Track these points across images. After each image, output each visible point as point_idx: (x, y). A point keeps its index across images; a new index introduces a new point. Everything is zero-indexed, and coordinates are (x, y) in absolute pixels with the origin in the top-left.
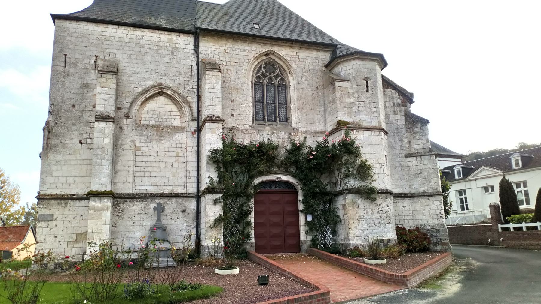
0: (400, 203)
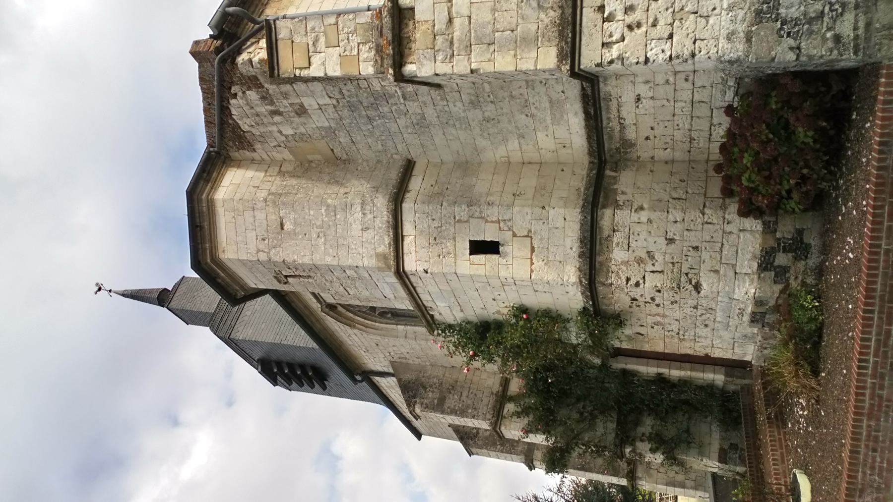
0: (624, 114)
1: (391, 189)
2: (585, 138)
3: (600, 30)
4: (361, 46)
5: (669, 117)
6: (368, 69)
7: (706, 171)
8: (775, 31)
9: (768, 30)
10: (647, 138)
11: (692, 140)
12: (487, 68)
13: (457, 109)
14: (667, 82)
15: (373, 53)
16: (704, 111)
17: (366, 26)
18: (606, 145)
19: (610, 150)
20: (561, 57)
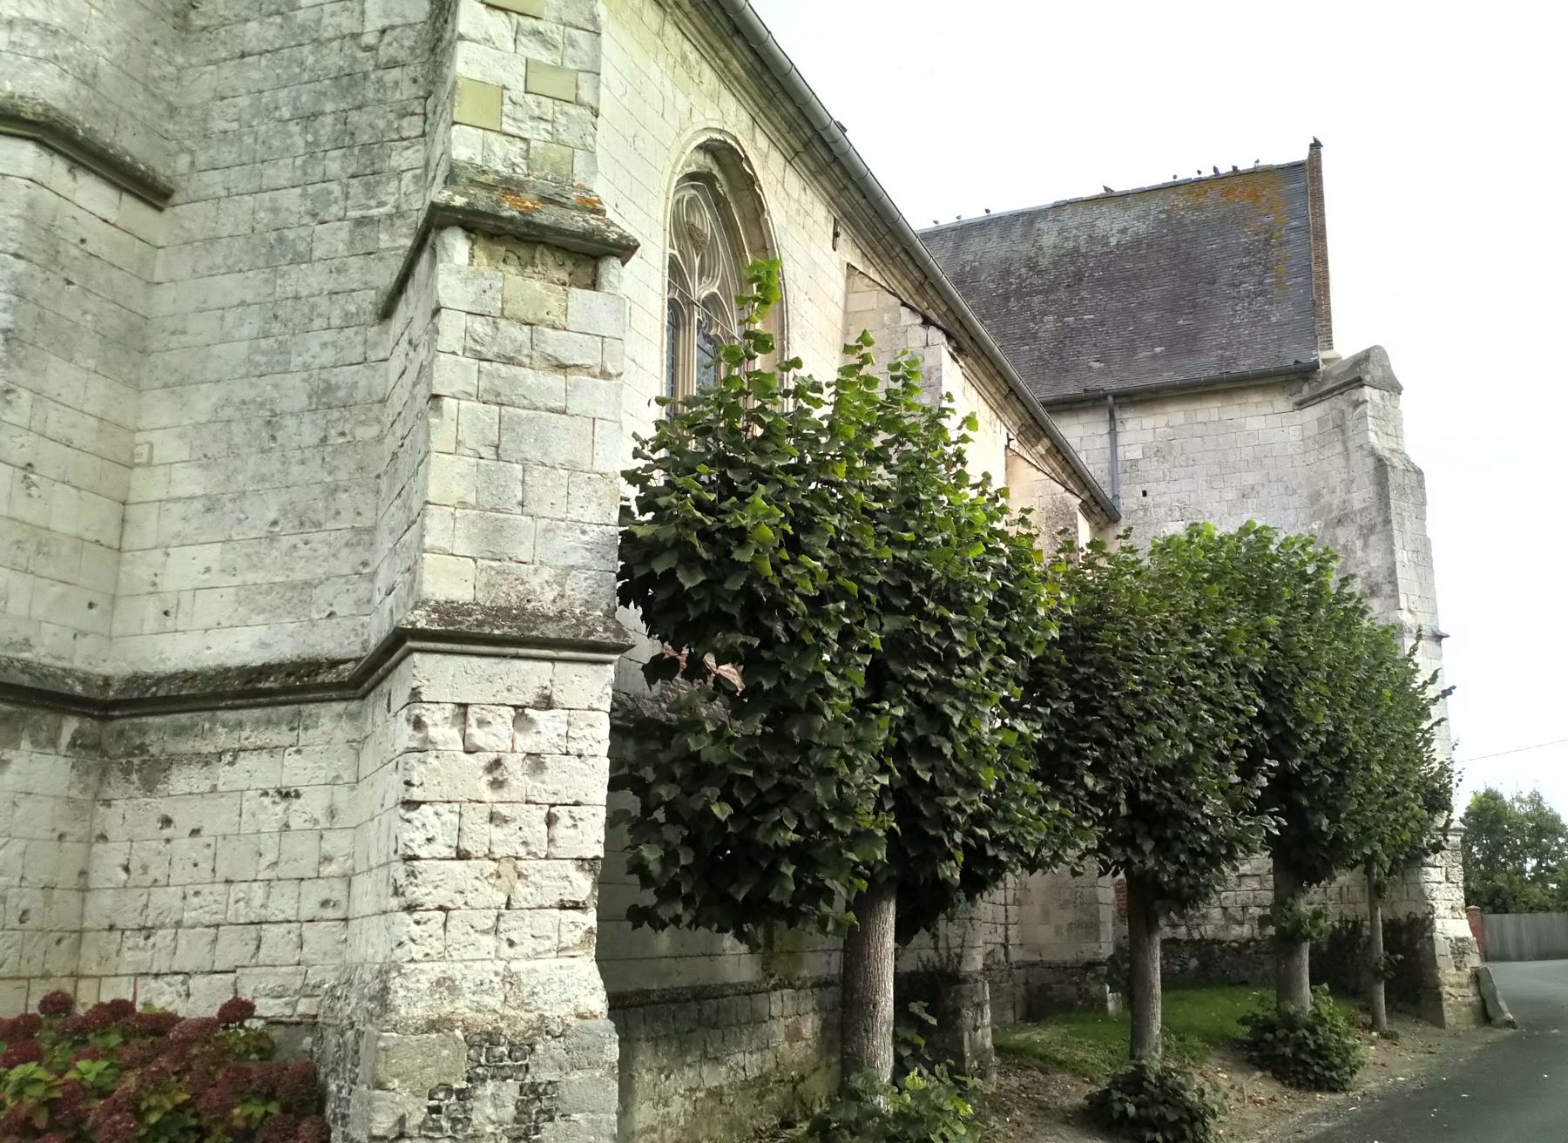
0: (247, 762)
1: (85, 123)
2: (190, 666)
3: (499, 699)
4: (522, 145)
5: (223, 871)
6: (464, 146)
7: (46, 976)
8: (446, 1080)
9: (451, 1062)
10: (167, 822)
11: (147, 931)
12: (442, 434)
13: (316, 349)
14: (327, 859)
15: (505, 171)
16: (232, 949)
17: (565, 170)
18: (158, 720)
19: (143, 732)
20: (448, 610)
